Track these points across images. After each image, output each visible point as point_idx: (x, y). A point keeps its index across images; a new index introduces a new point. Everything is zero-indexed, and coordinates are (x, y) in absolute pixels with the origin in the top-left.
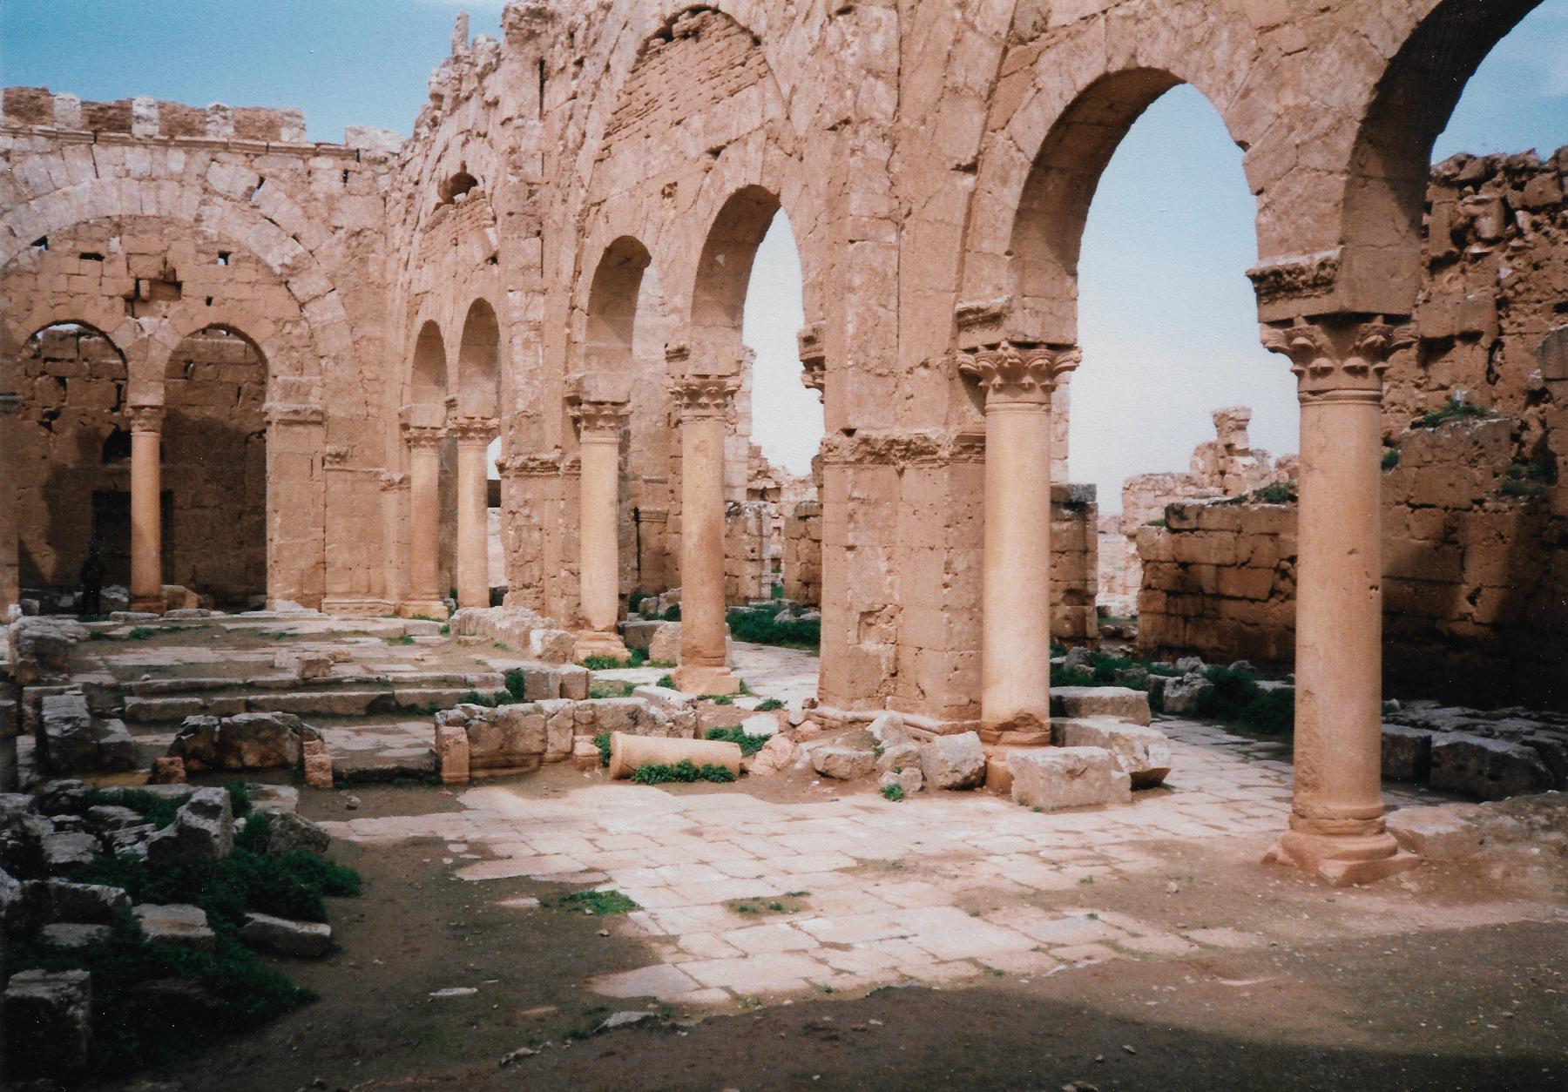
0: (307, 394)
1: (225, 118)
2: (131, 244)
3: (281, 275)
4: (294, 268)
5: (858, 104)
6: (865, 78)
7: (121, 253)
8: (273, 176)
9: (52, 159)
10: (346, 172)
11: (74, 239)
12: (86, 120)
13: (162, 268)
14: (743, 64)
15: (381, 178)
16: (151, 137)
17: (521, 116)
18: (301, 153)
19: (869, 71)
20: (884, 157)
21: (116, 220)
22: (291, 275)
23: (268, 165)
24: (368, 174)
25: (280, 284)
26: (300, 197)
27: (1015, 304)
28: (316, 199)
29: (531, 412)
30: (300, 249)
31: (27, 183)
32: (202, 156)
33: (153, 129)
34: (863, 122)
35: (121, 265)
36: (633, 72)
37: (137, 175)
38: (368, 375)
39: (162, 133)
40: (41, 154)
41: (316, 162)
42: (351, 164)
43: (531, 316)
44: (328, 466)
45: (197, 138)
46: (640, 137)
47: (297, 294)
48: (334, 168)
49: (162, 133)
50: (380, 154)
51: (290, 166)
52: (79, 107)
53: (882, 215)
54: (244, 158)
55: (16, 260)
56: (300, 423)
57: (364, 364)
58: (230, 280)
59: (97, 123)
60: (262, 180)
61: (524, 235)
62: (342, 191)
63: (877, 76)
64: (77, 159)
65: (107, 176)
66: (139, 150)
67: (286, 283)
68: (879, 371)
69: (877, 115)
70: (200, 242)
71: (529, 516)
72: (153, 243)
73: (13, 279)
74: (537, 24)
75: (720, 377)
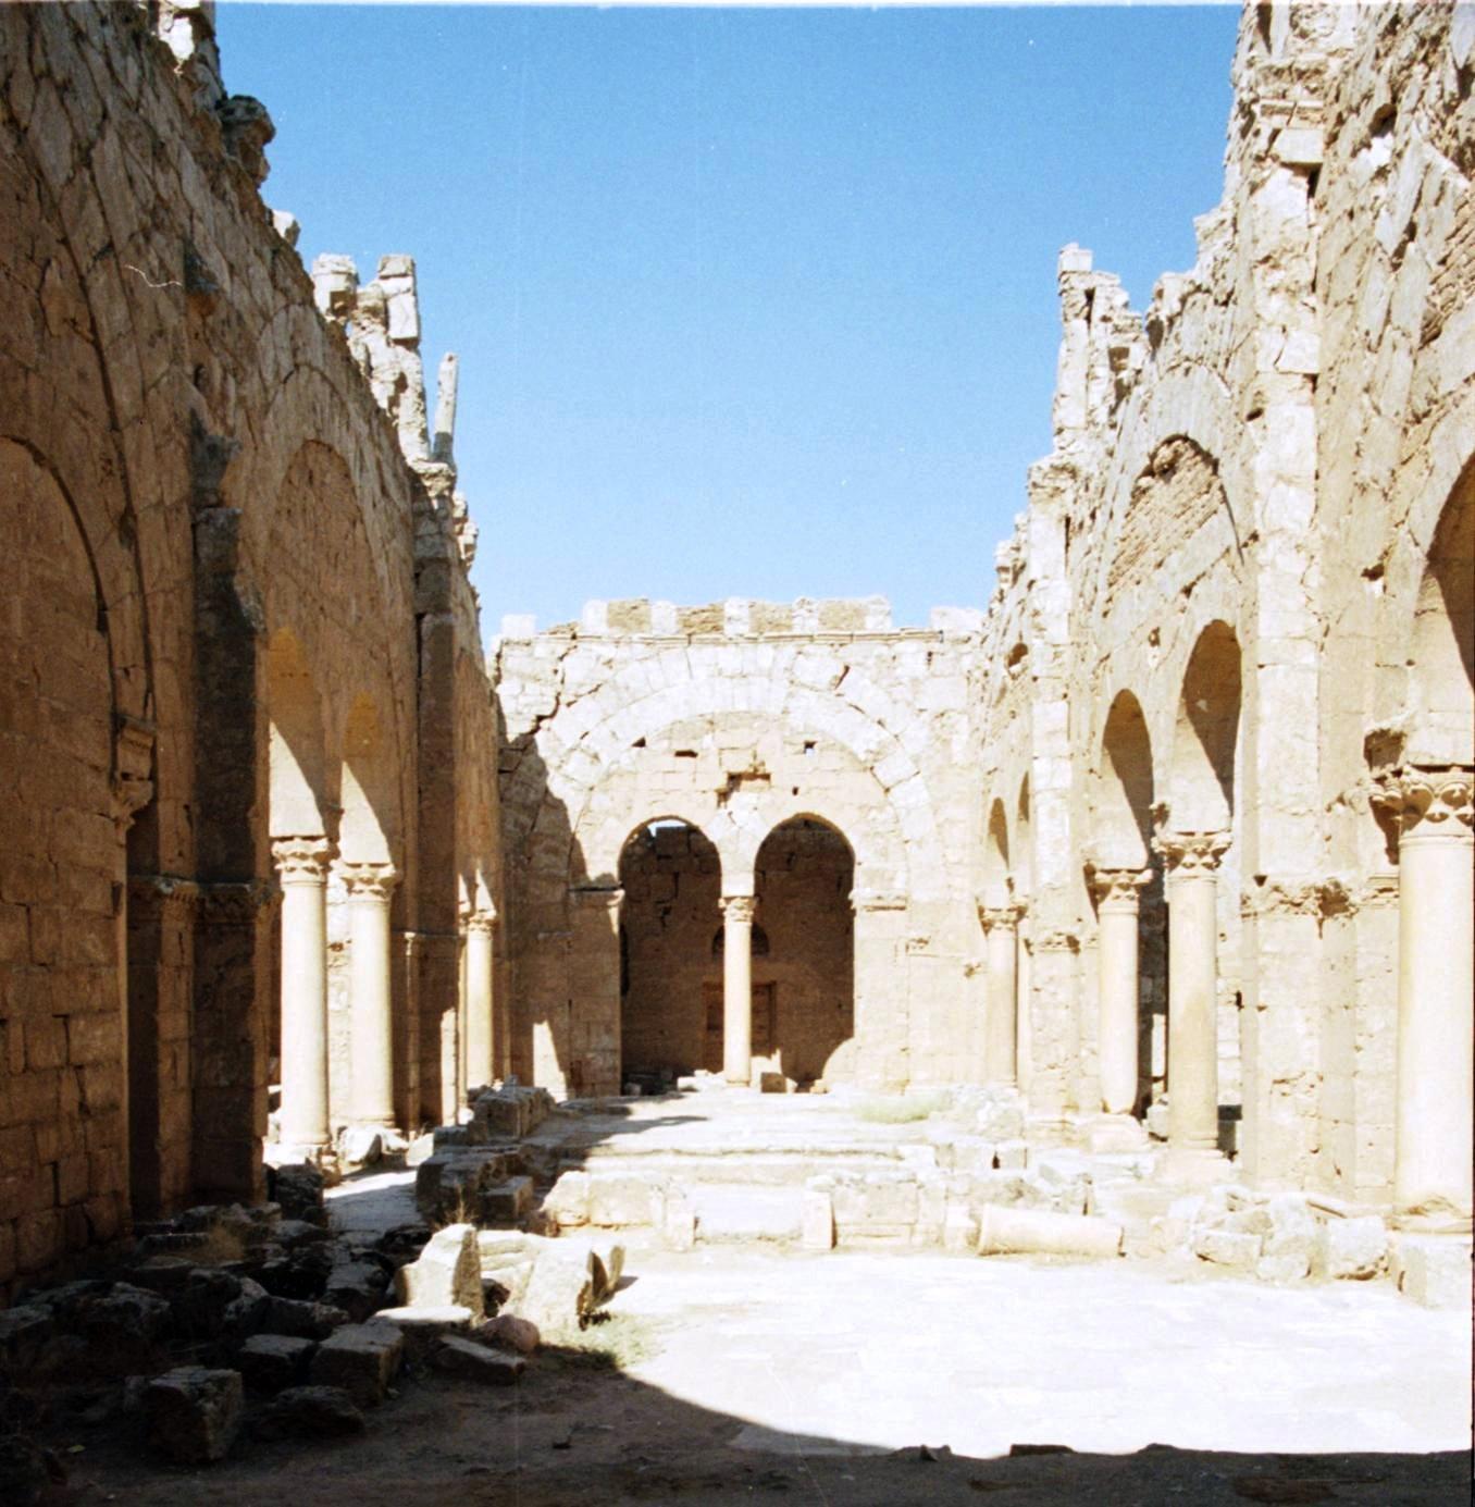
0: (892, 879)
1: (810, 611)
2: (725, 740)
3: (866, 761)
4: (878, 753)
5: (1267, 515)
6: (1274, 485)
7: (714, 749)
8: (859, 664)
9: (650, 664)
10: (930, 654)
11: (670, 738)
12: (680, 626)
13: (751, 761)
14: (1207, 492)
15: (965, 658)
16: (741, 635)
17: (1046, 577)
18: (887, 639)
19: (1280, 477)
20: (1298, 571)
21: (709, 717)
22: (875, 761)
23: (852, 653)
24: (951, 655)
25: (865, 770)
26: (885, 683)
27: (1418, 721)
28: (900, 684)
29: (1057, 884)
30: (885, 735)
31: (627, 688)
32: (790, 649)
33: (745, 630)
34: (1272, 533)
35: (713, 759)
36: (1127, 516)
37: (729, 674)
38: (952, 858)
39: (752, 631)
40: (640, 660)
41: (899, 647)
42: (935, 646)
43: (1056, 784)
44: (911, 951)
45: (784, 633)
46: (1131, 584)
47: (882, 780)
48: (918, 652)
49: (752, 631)
50: (964, 634)
51: (876, 652)
52: (675, 614)
53: (1297, 635)
54: (830, 649)
55: (618, 762)
56: (883, 908)
57: (947, 847)
58: (816, 769)
59: (691, 627)
60: (847, 669)
61: (1049, 698)
62: (927, 674)
63: (1289, 482)
64: (674, 660)
65: (701, 674)
66: (732, 648)
67: (872, 768)
68: (1294, 810)
69: (1289, 525)
70: (787, 734)
71: (1055, 994)
72: (740, 737)
73: (614, 780)
74: (1062, 480)
75: (1207, 834)
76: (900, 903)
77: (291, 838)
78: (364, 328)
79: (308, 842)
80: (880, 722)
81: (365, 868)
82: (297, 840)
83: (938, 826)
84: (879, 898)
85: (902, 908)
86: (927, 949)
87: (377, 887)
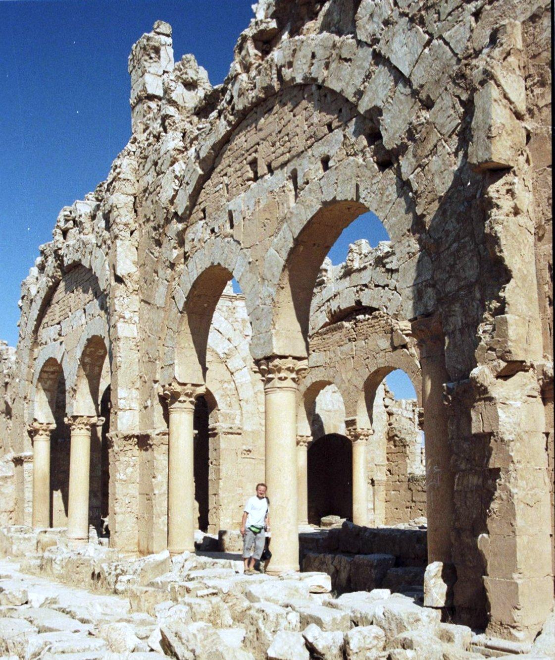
30: (231, 346)
41: (237, 303)
56: (232, 433)
57: (259, 404)
76: (239, 431)
77: (285, 357)
78: (151, 58)
79: (296, 361)
80: (228, 340)
81: (189, 386)
82: (290, 358)
83: (256, 393)
84: (231, 428)
85: (240, 434)
86: (251, 455)
87: (193, 399)
